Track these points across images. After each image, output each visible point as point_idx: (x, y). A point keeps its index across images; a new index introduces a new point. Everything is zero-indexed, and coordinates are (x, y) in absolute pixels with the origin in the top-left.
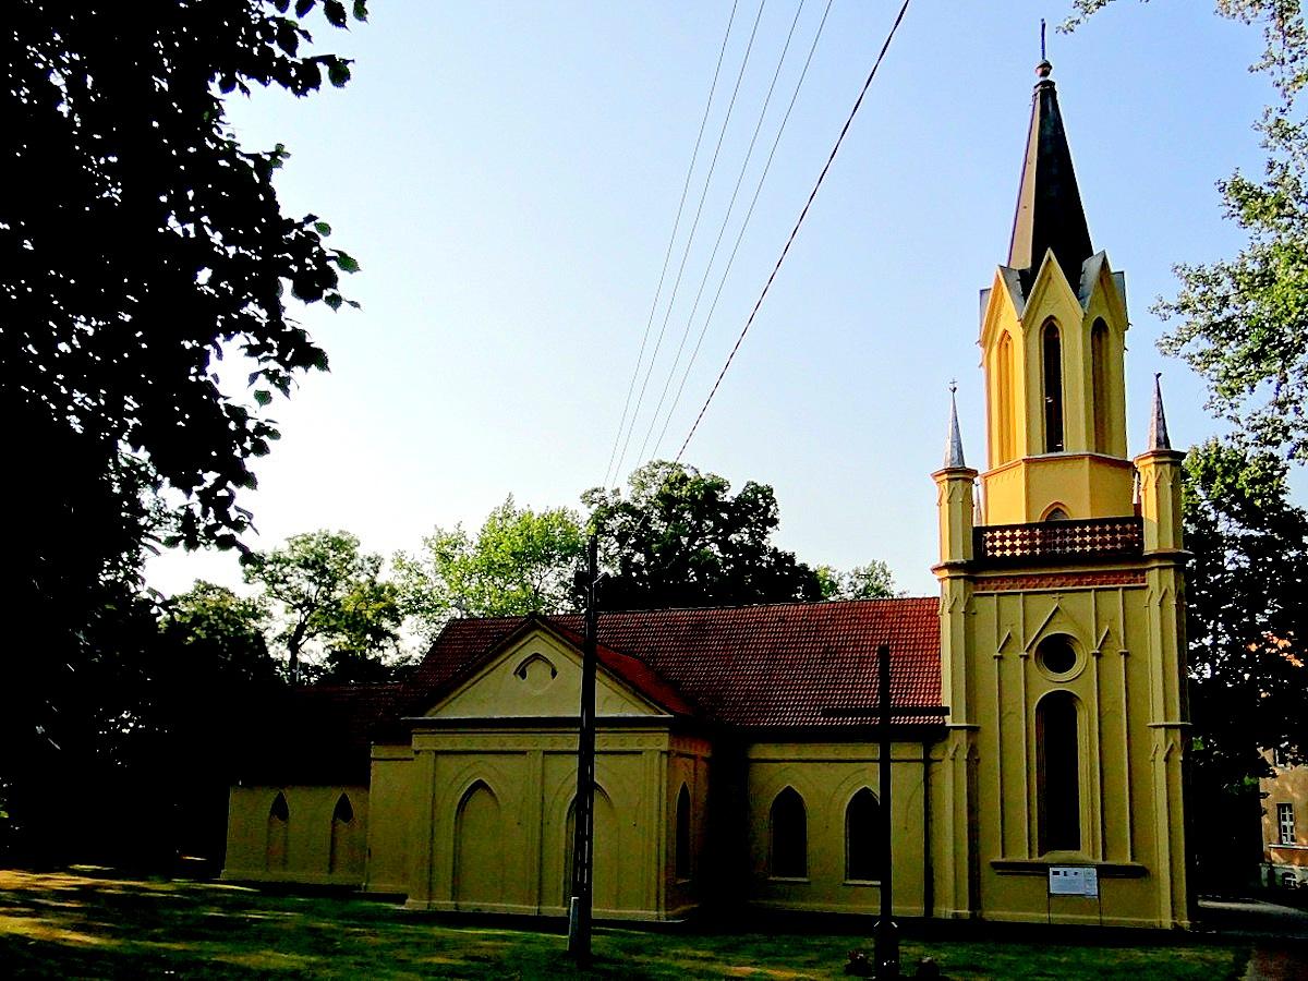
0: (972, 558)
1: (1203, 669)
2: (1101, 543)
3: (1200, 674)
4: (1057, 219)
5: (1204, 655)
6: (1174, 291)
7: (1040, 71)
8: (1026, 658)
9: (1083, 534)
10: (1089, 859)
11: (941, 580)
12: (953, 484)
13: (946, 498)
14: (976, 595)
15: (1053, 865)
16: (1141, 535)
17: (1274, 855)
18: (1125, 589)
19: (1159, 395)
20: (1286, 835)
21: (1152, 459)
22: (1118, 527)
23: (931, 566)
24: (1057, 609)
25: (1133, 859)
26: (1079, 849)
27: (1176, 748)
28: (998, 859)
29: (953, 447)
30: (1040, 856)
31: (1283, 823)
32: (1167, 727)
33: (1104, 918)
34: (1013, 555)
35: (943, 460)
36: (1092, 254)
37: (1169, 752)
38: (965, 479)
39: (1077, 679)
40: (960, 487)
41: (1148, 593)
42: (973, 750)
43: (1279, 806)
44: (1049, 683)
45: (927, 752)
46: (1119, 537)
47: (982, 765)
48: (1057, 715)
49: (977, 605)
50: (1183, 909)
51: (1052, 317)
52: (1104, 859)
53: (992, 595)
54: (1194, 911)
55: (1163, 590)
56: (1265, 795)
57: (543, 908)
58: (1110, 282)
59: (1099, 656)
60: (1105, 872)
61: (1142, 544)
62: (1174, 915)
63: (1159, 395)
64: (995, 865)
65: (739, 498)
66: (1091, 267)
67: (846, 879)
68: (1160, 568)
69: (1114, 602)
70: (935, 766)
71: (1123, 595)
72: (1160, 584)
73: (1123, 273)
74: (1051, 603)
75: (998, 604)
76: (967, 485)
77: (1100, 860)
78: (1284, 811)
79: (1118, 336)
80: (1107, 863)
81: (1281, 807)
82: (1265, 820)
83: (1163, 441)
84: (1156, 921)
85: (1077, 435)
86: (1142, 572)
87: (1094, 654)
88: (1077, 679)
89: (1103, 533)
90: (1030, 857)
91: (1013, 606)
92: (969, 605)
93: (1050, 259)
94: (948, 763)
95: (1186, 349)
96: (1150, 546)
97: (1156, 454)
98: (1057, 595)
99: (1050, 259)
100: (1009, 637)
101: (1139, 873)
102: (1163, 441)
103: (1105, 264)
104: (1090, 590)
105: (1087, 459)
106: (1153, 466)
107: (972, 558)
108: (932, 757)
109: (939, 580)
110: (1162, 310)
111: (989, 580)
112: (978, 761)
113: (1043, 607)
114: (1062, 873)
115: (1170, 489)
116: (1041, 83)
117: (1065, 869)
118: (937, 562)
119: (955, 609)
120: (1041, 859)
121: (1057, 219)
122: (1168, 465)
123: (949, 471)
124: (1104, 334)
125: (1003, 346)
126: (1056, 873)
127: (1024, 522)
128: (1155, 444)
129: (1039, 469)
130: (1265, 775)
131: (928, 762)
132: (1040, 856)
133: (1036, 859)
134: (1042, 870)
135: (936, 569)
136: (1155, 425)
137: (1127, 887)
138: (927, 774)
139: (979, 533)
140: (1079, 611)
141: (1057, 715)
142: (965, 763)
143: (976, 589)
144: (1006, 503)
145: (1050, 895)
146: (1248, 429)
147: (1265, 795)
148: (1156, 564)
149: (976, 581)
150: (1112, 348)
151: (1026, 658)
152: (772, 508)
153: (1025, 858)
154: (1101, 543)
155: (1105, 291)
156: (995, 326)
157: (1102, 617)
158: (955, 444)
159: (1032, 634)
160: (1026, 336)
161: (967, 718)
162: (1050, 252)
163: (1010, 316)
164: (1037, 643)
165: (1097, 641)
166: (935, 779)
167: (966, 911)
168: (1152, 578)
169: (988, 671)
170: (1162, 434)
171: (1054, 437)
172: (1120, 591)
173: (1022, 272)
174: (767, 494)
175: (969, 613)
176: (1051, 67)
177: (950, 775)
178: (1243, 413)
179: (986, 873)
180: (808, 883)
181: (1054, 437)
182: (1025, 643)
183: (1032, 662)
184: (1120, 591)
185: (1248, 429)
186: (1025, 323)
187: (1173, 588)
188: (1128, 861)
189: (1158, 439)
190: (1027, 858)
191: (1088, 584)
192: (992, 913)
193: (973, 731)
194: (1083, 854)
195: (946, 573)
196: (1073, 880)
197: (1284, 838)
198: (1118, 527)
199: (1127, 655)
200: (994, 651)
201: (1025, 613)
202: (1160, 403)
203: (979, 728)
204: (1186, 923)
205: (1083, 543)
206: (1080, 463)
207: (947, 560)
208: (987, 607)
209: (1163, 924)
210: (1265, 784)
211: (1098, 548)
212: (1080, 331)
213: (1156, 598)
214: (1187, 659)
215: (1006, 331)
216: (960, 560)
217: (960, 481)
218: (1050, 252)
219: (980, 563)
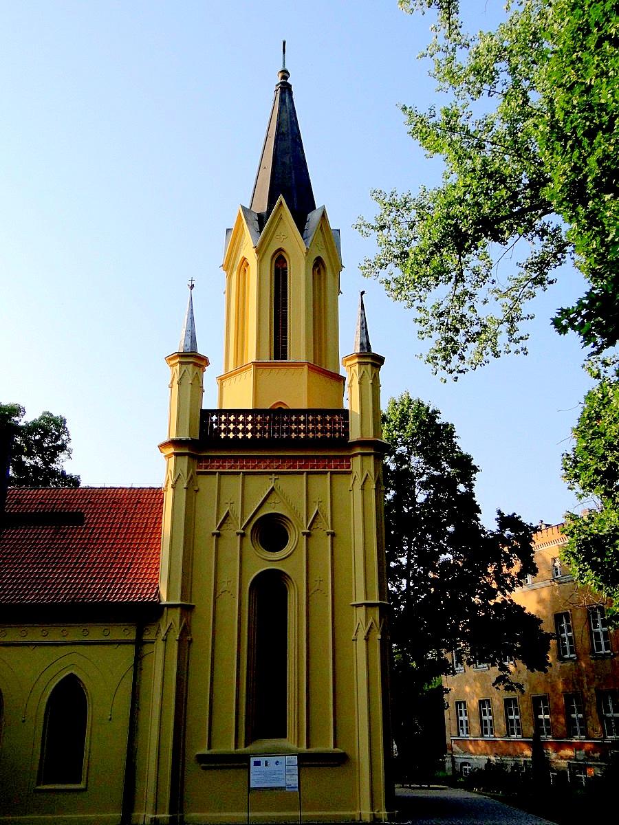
0: (197, 438)
1: (401, 584)
2: (313, 431)
3: (398, 587)
4: (289, 178)
5: (402, 572)
6: (373, 212)
7: (280, 75)
8: (243, 535)
9: (298, 422)
10: (293, 746)
11: (168, 457)
12: (184, 367)
13: (176, 379)
14: (199, 473)
15: (256, 755)
16: (347, 425)
17: (454, 746)
18: (332, 473)
19: (363, 308)
20: (462, 729)
21: (356, 360)
22: (328, 418)
23: (158, 444)
24: (273, 489)
25: (335, 746)
26: (285, 737)
27: (375, 628)
28: (205, 751)
29: (186, 335)
30: (246, 746)
31: (460, 718)
32: (368, 605)
33: (251, 814)
34: (236, 438)
35: (178, 344)
36: (315, 208)
37: (369, 631)
38: (195, 364)
39: (289, 559)
40: (190, 370)
41: (352, 477)
42: (186, 631)
43: (457, 703)
44: (261, 561)
45: (140, 634)
46: (328, 426)
47: (194, 648)
48: (269, 593)
49: (199, 483)
50: (382, 799)
51: (280, 250)
52: (308, 747)
53: (214, 473)
54: (392, 801)
55: (365, 474)
56: (447, 691)
57: (251, 814)
58: (330, 238)
59: (308, 535)
60: (307, 761)
61: (347, 434)
62: (372, 808)
63: (363, 308)
64: (201, 759)
65: (34, 423)
66: (314, 217)
67: (38, 784)
68: (363, 455)
69: (322, 485)
70: (147, 649)
71: (331, 477)
72: (362, 469)
73: (339, 230)
74: (266, 484)
75: (219, 483)
76: (197, 369)
77: (304, 749)
78: (460, 708)
79: (334, 276)
80: (312, 750)
81: (459, 704)
82: (447, 713)
83: (365, 346)
84: (356, 813)
85: (298, 348)
86: (348, 458)
87: (304, 534)
88: (289, 559)
89: (315, 422)
90: (236, 747)
91: (233, 485)
92: (191, 481)
93: (281, 203)
94: (160, 645)
95: (384, 274)
96: (355, 435)
97: (360, 356)
98: (273, 477)
99: (281, 203)
100: (227, 515)
101: (339, 760)
102: (365, 346)
103: (324, 215)
104: (301, 473)
105: (306, 366)
106: (357, 365)
107: (197, 438)
108: (145, 638)
109: (165, 456)
110: (363, 228)
111: (213, 458)
112: (190, 642)
113: (259, 487)
114: (263, 764)
115: (370, 386)
116: (281, 83)
117: (266, 759)
118: (166, 439)
119: (177, 486)
120: (248, 748)
121: (289, 178)
122: (369, 366)
123: (181, 355)
124: (324, 268)
125: (242, 270)
126: (257, 763)
127: (249, 406)
128: (358, 348)
129: (265, 373)
130: (447, 673)
131: (139, 644)
132: (246, 746)
133: (242, 749)
134: (240, 762)
135: (163, 446)
136: (359, 333)
137: (326, 777)
138: (139, 658)
139: (206, 414)
140: (293, 493)
141: (269, 593)
142: (176, 643)
143: (200, 467)
144: (231, 391)
145: (250, 789)
146: (432, 315)
147: (447, 691)
148: (358, 451)
149: (200, 459)
150: (329, 293)
151: (243, 535)
152: (64, 437)
153: (231, 749)
154: (313, 431)
155: (323, 236)
156: (236, 255)
157: (311, 500)
158: (189, 333)
159: (249, 514)
160: (260, 261)
161: (181, 598)
162: (281, 198)
163: (248, 250)
164: (253, 522)
165: (307, 520)
166: (146, 663)
167: (167, 815)
168: (356, 463)
169: (205, 546)
170: (365, 340)
171: (280, 349)
172: (329, 473)
173: (259, 215)
174: (60, 424)
175: (192, 490)
176: (289, 74)
177: (160, 656)
178: (429, 304)
179: (192, 768)
180: (85, 790)
181: (280, 349)
182: (242, 520)
183: (248, 540)
184: (329, 473)
185: (432, 315)
186: (259, 250)
187: (373, 474)
188: (330, 748)
189: (361, 344)
190: (233, 749)
191: (300, 468)
192: (193, 814)
193: (187, 610)
194: (289, 743)
195: (172, 450)
196: (274, 770)
197: (461, 731)
198: (328, 418)
199: (333, 535)
200: (213, 529)
201: (244, 493)
202: (363, 315)
203: (194, 606)
204: (383, 814)
205: (301, 431)
206: (298, 371)
207: (174, 437)
208: (209, 484)
209: (363, 818)
210: (446, 681)
211: (311, 435)
212: (303, 262)
213: (359, 483)
214: (387, 574)
215: (245, 259)
216: (185, 436)
217: (191, 365)
218: (281, 198)
219: (205, 443)
